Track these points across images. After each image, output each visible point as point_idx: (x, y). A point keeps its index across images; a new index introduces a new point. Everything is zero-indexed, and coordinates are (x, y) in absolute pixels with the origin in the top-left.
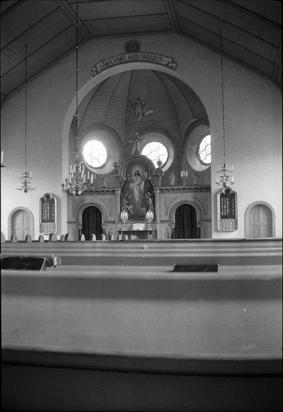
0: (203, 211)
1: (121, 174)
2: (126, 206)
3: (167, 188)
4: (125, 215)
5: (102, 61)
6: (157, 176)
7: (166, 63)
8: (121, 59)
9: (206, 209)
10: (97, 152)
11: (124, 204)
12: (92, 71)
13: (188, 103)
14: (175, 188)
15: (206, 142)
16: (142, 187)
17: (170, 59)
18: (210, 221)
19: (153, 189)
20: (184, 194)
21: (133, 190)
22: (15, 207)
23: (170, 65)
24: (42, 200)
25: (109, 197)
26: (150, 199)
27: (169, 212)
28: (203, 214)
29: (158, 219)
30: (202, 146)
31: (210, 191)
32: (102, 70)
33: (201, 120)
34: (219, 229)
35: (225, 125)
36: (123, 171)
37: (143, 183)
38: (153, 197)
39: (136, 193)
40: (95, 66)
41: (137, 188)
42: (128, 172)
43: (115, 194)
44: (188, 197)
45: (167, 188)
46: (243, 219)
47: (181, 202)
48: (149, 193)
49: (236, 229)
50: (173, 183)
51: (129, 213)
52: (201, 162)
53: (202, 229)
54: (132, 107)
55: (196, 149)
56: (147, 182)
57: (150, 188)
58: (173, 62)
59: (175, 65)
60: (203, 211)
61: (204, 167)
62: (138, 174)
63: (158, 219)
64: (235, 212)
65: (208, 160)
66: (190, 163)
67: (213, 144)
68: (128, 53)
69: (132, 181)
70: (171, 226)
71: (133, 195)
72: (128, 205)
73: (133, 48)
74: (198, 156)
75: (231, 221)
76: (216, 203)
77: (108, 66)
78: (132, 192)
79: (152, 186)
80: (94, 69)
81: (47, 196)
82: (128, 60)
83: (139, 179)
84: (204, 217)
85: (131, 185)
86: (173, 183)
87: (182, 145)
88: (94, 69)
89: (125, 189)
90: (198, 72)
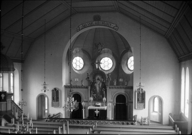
0: (129, 98)
1: (91, 79)
2: (93, 94)
3: (112, 86)
4: (92, 99)
5: (82, 24)
6: (108, 80)
7: (113, 27)
8: (91, 24)
9: (131, 98)
10: (78, 63)
11: (92, 93)
12: (77, 29)
13: (123, 41)
14: (116, 87)
15: (132, 59)
16: (101, 86)
17: (115, 25)
18: (132, 103)
19: (106, 87)
20: (120, 90)
21: (96, 87)
22: (38, 94)
23: (115, 28)
24: (53, 91)
25: (85, 89)
26: (104, 91)
27: (113, 98)
28: (129, 99)
29: (108, 101)
30: (129, 61)
31: (133, 89)
32: (82, 29)
33: (128, 49)
34: (136, 108)
35: (141, 58)
36: (91, 77)
37: (101, 84)
38: (106, 91)
39: (98, 88)
40: (79, 27)
41: (98, 86)
42: (94, 78)
43: (88, 88)
44: (122, 91)
45: (112, 86)
46: (148, 103)
47: (118, 93)
48: (103, 89)
49: (145, 108)
50: (115, 84)
51: (94, 97)
52: (129, 69)
53: (128, 106)
54: (96, 46)
55: (126, 62)
56: (103, 83)
57: (104, 87)
58: (116, 26)
59: (117, 28)
60: (129, 98)
61: (130, 71)
62: (99, 79)
63: (108, 101)
64: (144, 97)
65: (132, 68)
66: (123, 69)
67: (135, 61)
68: (95, 21)
69: (96, 83)
70: (114, 105)
71: (96, 90)
72: (94, 94)
73: (97, 19)
74: (127, 65)
75: (142, 104)
76: (136, 96)
77: (85, 27)
78: (95, 88)
79: (105, 86)
80: (78, 28)
81: (55, 89)
82: (95, 24)
83: (99, 82)
84: (129, 101)
85: (96, 84)
86: (115, 84)
87: (119, 61)
88: (78, 28)
89: (92, 85)
90: (128, 32)
